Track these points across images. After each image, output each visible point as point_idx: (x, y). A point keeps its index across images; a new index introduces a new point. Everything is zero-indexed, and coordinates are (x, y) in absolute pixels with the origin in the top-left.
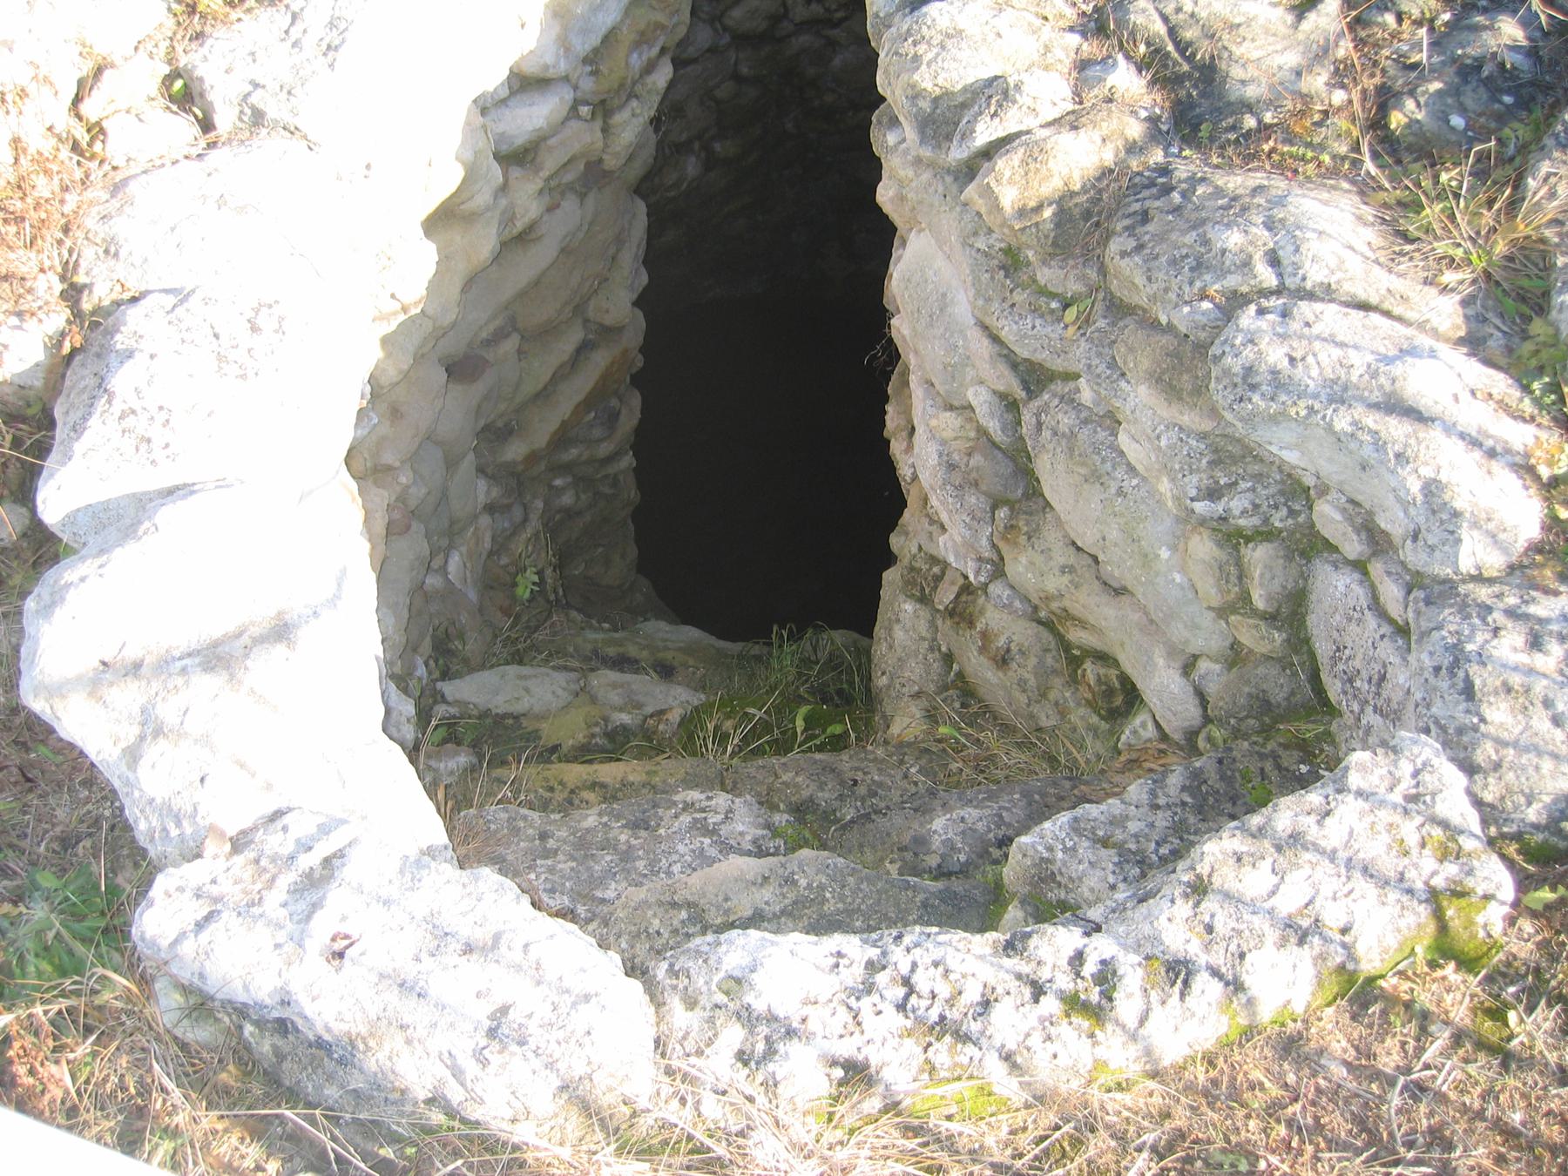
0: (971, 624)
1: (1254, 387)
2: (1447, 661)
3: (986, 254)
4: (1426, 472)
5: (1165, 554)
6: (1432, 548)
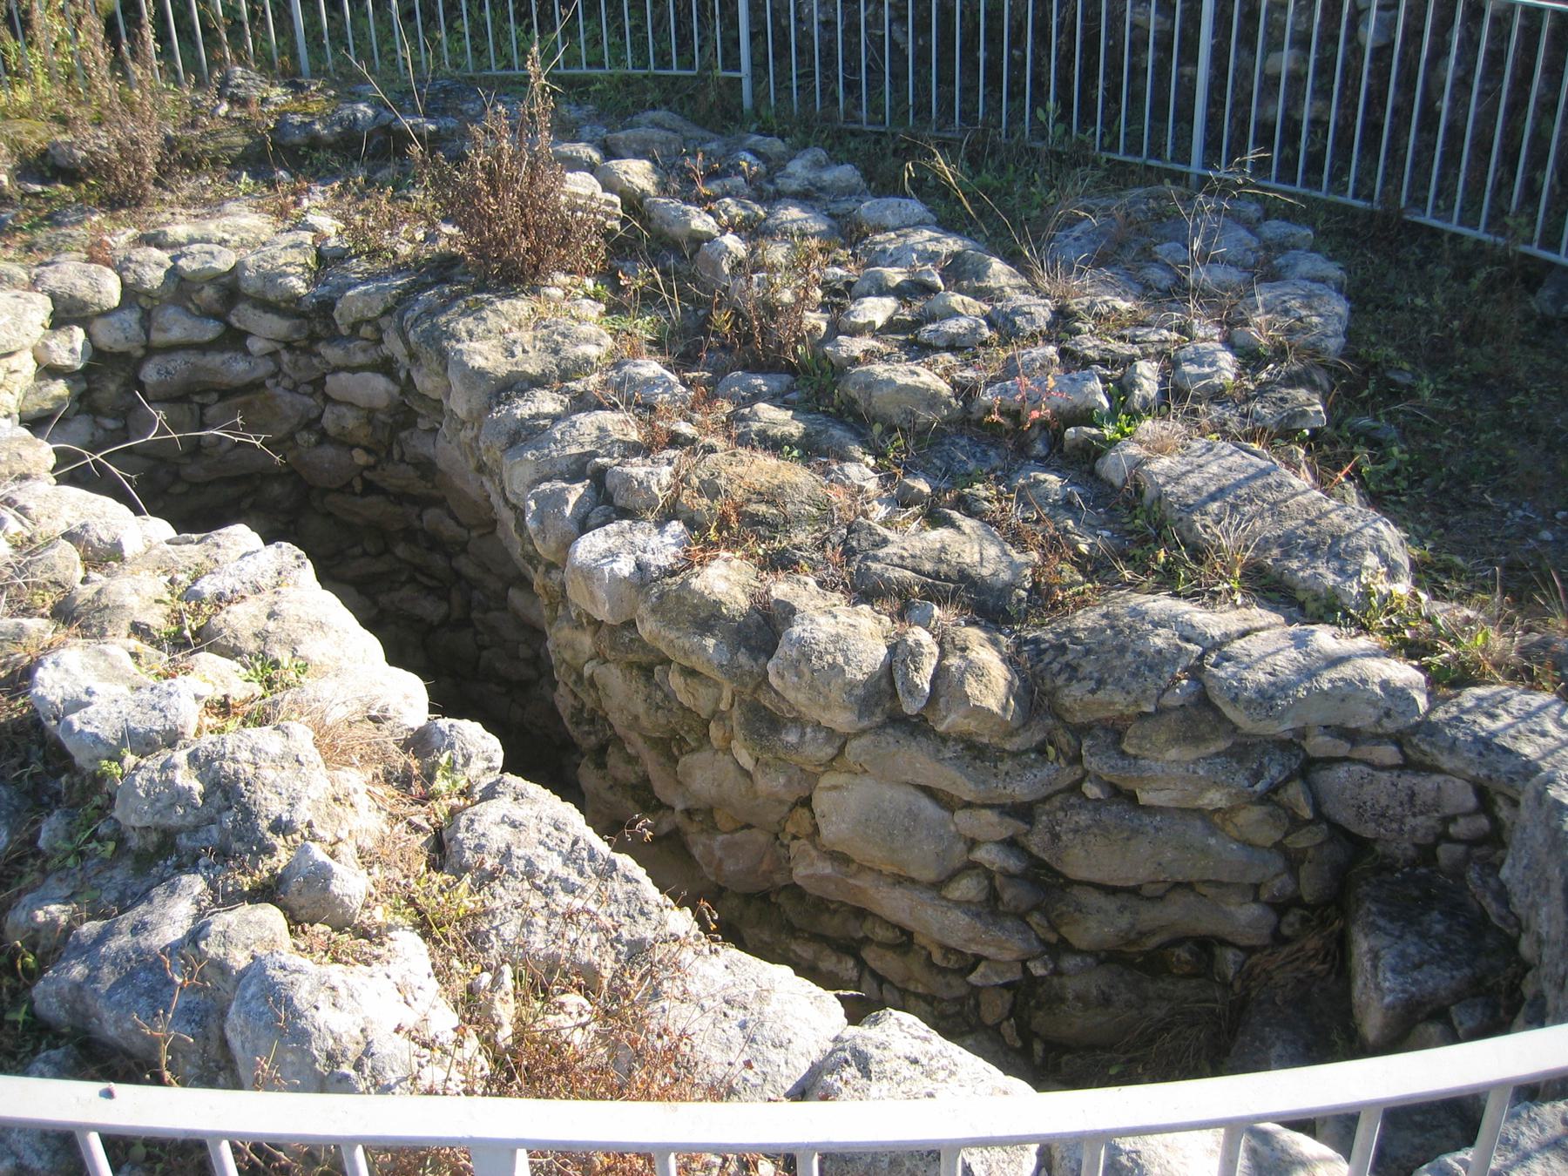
0: (1062, 1000)
1: (1272, 698)
2: (1481, 747)
3: (957, 758)
4: (1377, 680)
5: (1212, 841)
6: (1403, 713)
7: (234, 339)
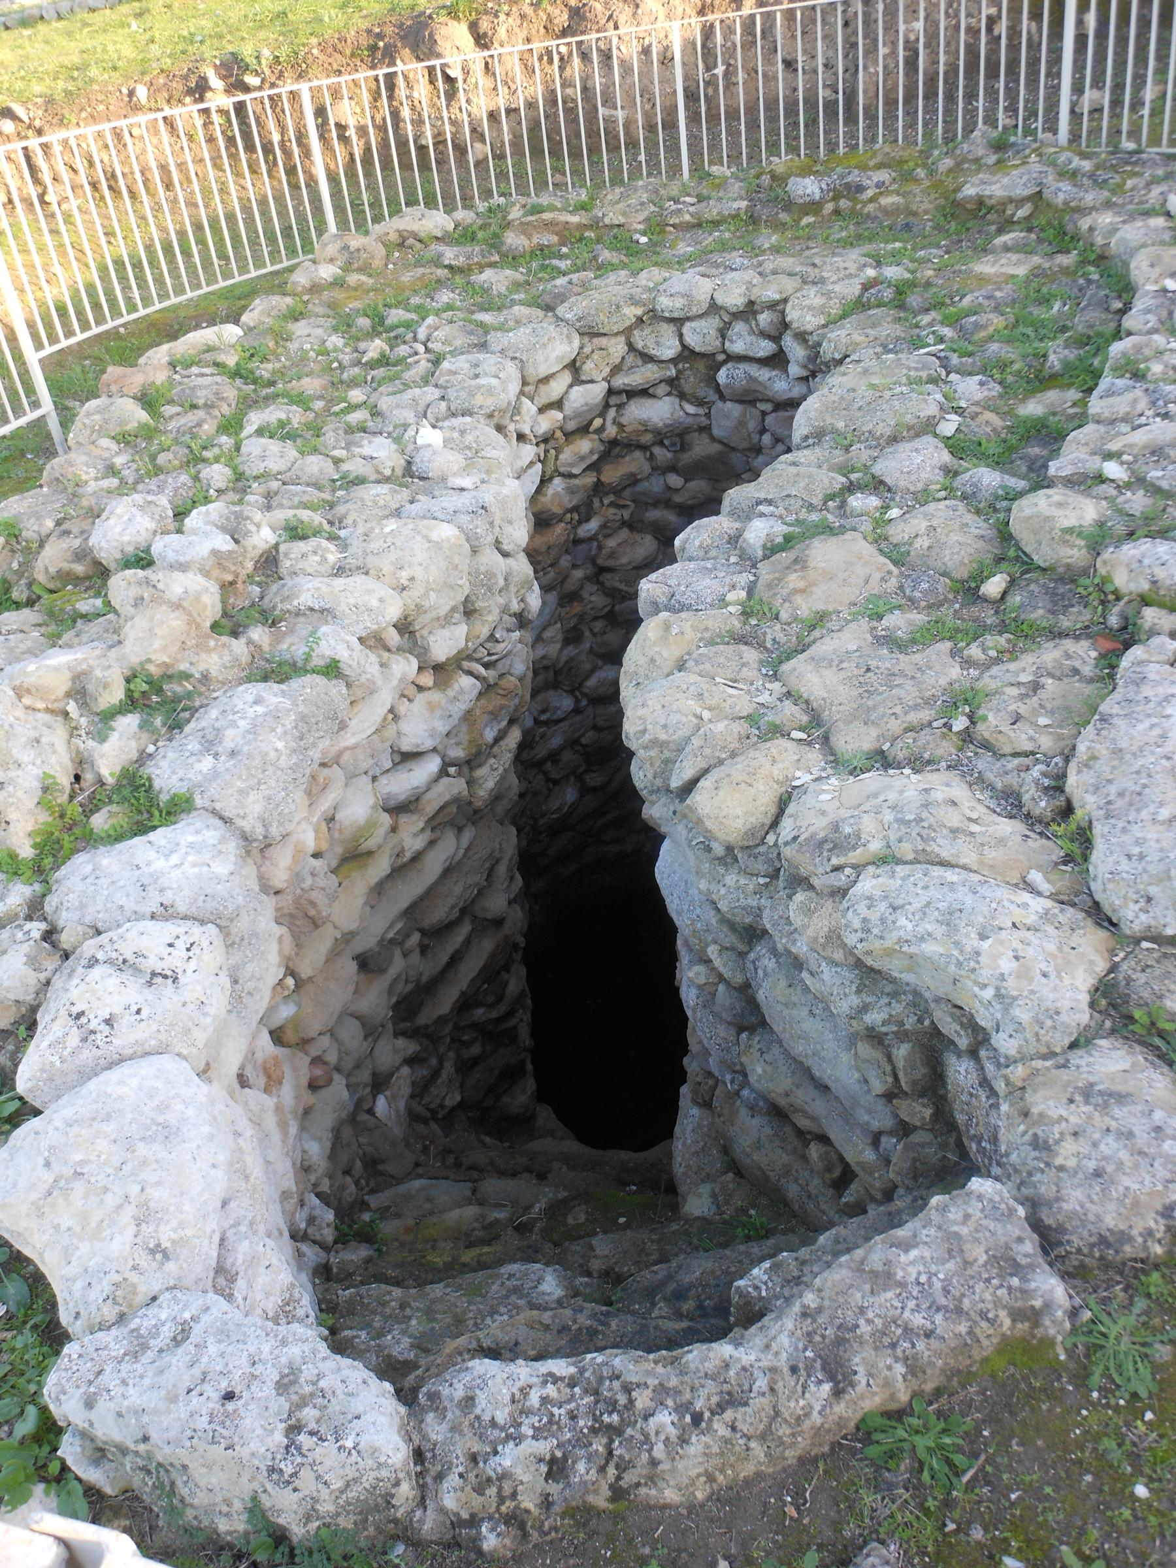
7: (778, 360)
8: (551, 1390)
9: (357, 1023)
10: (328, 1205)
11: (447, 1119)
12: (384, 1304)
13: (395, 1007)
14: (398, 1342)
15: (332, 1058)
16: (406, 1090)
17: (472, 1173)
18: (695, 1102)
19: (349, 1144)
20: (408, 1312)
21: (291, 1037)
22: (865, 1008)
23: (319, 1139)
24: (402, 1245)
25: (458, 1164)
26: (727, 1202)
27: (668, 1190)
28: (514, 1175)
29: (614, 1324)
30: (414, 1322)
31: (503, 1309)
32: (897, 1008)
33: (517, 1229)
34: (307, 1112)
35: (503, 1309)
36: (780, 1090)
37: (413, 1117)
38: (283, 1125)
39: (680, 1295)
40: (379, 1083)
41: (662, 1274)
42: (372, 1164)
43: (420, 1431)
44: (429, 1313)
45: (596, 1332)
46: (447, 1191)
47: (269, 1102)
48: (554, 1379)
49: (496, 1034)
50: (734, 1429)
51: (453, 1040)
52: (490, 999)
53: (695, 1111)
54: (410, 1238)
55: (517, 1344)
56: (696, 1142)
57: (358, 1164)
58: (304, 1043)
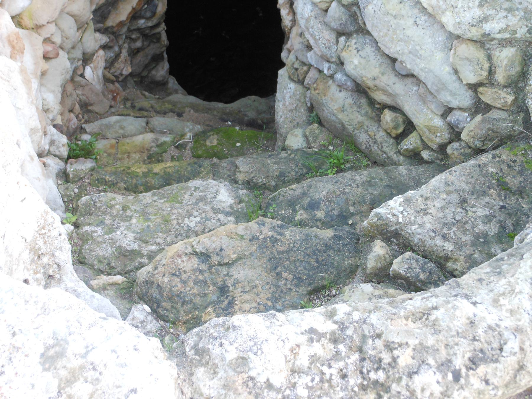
8: (317, 349)
9: (72, 20)
10: (61, 132)
11: (124, 81)
12: (111, 207)
13: (95, 12)
14: (125, 236)
15: (58, 39)
16: (102, 64)
17: (141, 112)
18: (291, 79)
19: (71, 95)
20: (129, 213)
21: (26, 21)
22: (486, 19)
23: (53, 92)
24: (109, 155)
25: (133, 107)
26: (315, 141)
27: (264, 127)
28: (165, 113)
29: (287, 234)
30: (134, 221)
31: (195, 213)
32: (513, 20)
33: (177, 147)
34: (43, 74)
35: (195, 213)
36: (370, 76)
37: (107, 80)
38: (27, 82)
39: (313, 206)
40: (87, 59)
41: (299, 192)
42: (85, 106)
43: (192, 384)
44: (144, 214)
45: (276, 240)
46: (132, 123)
47: (15, 65)
48: (313, 335)
49: (148, 36)
50: (487, 382)
51: (126, 37)
52: (148, 14)
53: (292, 85)
54: (113, 151)
55: (221, 250)
56: (291, 104)
57: (77, 107)
58: (37, 28)
